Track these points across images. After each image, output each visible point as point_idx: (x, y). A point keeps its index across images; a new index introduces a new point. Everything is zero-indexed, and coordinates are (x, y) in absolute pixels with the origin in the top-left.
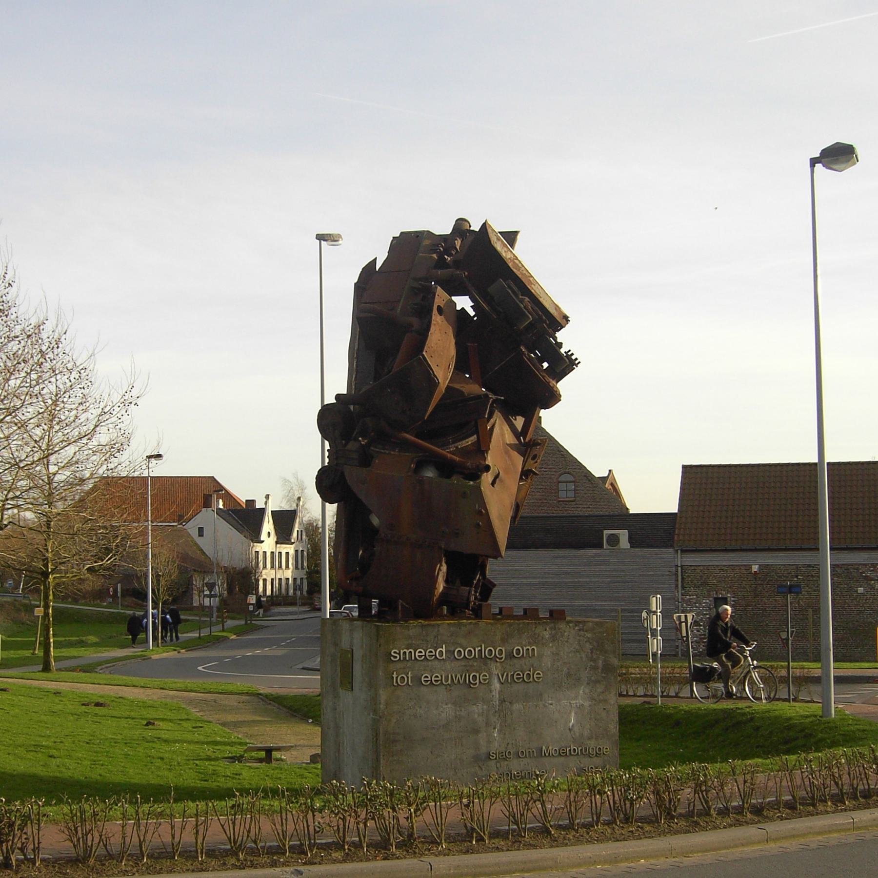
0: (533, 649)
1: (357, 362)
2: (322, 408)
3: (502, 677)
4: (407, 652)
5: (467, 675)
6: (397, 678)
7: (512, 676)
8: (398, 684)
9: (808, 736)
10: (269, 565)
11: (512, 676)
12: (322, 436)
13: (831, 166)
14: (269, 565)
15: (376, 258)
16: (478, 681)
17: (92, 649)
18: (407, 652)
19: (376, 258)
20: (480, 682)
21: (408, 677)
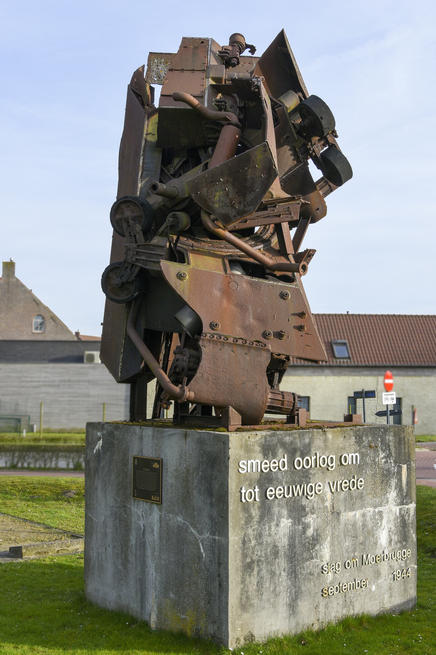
0: (357, 456)
1: (143, 160)
2: (117, 201)
3: (333, 487)
4: (254, 463)
5: (294, 486)
6: (245, 493)
7: (341, 484)
8: (246, 501)
9: (292, 538)
10: (339, 337)
11: (341, 484)
12: (115, 230)
13: (189, 107)
14: (339, 337)
15: (283, 29)
16: (313, 492)
17: (132, 462)
18: (254, 463)
19: (283, 29)
20: (316, 493)
21: (255, 492)
